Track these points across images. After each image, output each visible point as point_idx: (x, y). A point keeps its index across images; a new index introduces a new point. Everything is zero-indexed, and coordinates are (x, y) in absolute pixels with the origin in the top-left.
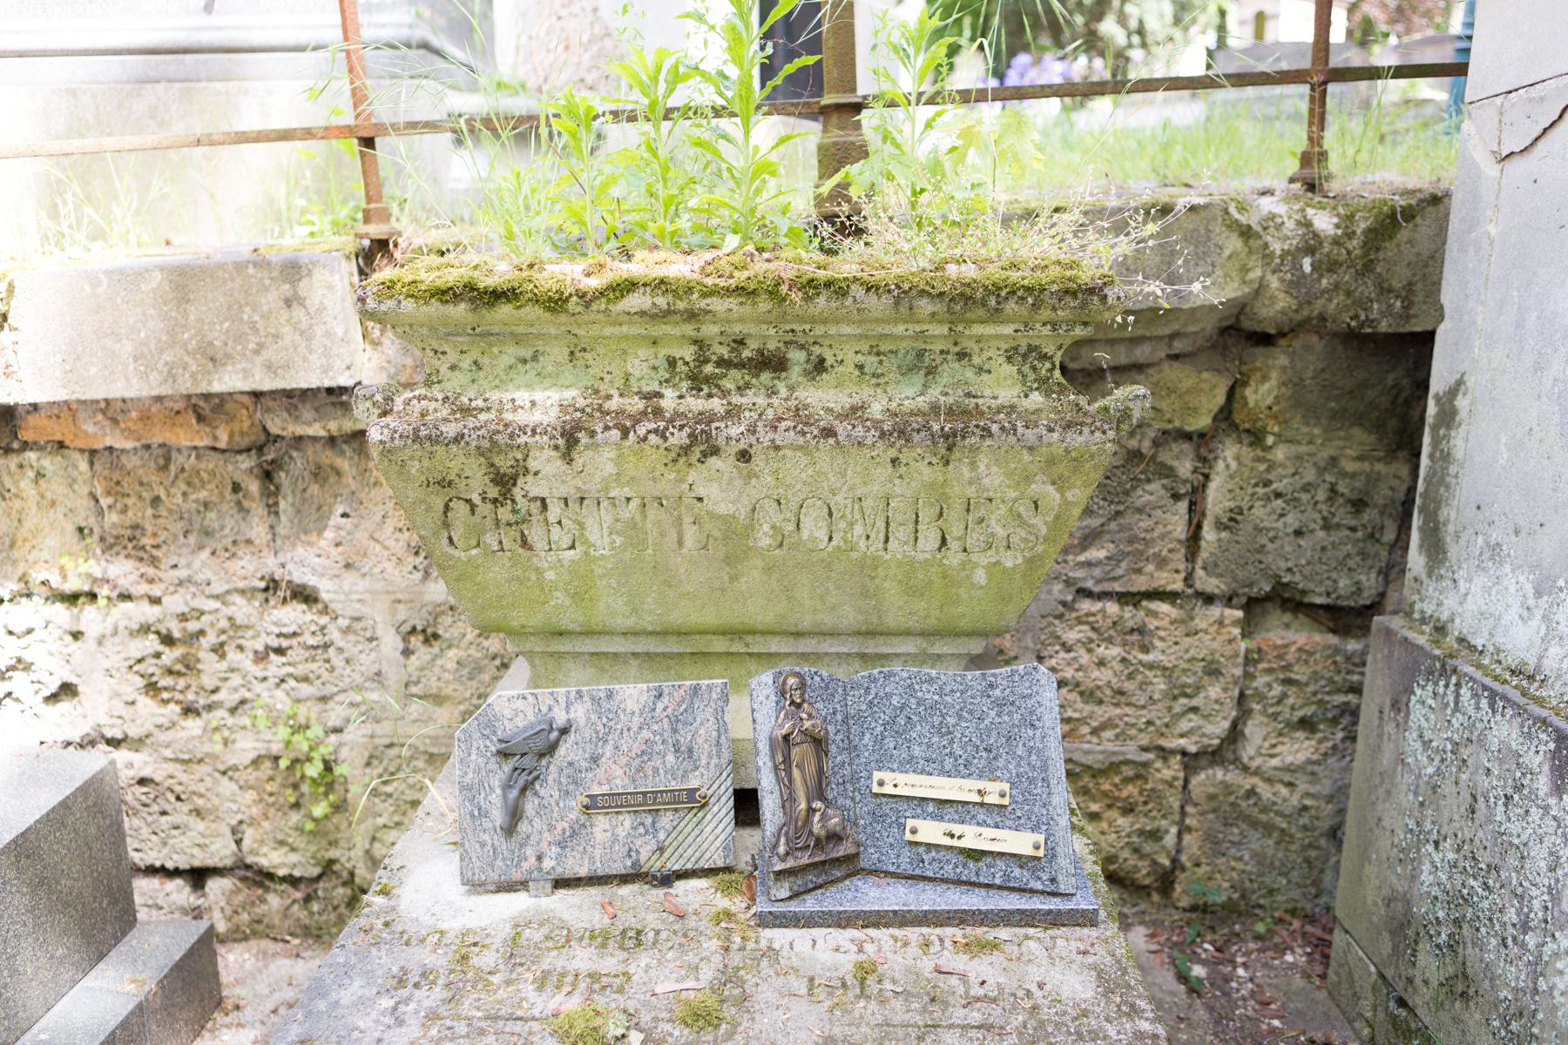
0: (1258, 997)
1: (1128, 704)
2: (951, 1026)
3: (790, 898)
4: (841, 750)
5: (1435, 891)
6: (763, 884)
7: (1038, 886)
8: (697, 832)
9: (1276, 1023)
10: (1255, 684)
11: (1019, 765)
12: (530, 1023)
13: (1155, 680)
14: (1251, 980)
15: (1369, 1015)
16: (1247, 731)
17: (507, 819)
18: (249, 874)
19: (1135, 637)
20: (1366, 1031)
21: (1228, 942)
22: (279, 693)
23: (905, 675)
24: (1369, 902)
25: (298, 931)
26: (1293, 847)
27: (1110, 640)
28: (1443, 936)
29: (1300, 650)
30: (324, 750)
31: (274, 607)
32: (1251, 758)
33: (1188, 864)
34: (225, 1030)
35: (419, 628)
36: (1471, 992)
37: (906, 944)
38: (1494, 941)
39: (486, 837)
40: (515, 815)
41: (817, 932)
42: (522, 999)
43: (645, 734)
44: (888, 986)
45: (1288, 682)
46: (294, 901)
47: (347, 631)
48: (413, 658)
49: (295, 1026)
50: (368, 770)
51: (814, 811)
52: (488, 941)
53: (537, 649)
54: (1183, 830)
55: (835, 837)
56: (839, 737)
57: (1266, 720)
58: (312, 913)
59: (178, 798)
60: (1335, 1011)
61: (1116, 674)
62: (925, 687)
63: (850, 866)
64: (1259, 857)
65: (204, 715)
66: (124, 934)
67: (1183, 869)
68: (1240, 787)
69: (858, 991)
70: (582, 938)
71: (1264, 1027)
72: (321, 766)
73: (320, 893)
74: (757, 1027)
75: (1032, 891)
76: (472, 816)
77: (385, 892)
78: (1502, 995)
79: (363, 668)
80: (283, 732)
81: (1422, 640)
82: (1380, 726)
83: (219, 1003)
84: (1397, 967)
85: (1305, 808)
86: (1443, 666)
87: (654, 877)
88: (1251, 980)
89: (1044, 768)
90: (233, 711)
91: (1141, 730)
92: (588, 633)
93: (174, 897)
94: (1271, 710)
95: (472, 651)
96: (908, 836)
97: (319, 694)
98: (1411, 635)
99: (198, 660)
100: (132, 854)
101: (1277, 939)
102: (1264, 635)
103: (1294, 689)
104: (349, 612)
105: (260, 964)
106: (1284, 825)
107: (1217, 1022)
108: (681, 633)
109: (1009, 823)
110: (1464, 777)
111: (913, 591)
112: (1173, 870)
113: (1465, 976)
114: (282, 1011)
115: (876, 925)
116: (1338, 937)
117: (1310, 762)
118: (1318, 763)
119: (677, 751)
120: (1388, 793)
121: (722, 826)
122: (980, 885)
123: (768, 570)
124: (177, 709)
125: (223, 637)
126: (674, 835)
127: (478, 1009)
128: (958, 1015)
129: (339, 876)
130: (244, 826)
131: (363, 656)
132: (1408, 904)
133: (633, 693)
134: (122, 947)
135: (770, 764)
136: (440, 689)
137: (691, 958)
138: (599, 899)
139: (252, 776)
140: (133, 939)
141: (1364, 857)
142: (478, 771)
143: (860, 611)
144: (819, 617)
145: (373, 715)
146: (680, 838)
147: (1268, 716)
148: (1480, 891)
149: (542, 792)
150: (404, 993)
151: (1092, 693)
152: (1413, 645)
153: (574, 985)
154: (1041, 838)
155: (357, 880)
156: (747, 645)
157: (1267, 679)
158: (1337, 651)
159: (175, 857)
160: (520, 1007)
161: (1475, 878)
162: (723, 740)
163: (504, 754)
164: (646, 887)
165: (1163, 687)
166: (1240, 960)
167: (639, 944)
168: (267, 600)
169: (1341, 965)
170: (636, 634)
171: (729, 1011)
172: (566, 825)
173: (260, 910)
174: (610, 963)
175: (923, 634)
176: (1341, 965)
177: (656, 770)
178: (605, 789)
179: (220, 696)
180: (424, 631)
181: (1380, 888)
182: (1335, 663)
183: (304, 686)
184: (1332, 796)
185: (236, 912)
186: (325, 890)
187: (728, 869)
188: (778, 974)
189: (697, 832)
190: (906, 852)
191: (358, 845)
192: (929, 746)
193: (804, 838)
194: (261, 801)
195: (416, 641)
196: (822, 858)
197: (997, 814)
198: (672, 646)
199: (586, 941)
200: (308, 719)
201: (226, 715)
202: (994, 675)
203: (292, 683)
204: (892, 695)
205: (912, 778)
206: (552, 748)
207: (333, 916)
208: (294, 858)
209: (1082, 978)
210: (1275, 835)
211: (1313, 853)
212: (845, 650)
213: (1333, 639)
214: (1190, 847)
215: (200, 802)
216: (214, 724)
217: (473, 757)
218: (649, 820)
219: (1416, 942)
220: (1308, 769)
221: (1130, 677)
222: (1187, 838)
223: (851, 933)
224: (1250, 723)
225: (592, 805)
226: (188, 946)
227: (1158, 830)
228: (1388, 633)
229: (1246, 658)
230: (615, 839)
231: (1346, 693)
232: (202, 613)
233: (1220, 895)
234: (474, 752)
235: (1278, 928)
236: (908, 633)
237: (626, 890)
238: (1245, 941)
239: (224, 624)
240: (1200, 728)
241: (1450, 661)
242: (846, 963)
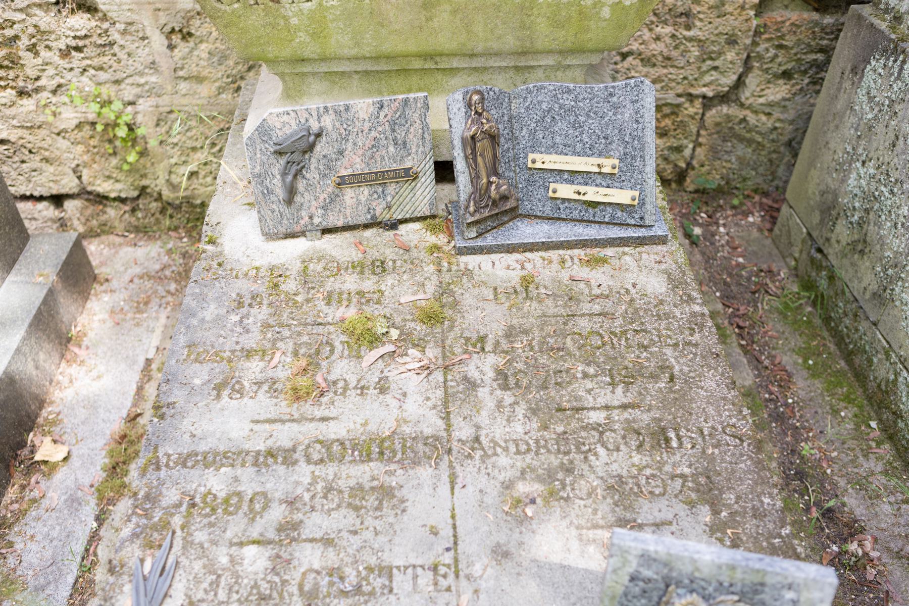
0: (731, 244)
1: (672, 66)
2: (583, 315)
3: (477, 237)
4: (507, 140)
5: (856, 191)
6: (457, 227)
7: (633, 222)
8: (411, 195)
9: (741, 260)
10: (758, 49)
11: (626, 147)
12: (328, 327)
13: (692, 49)
14: (727, 234)
15: (797, 255)
16: (747, 81)
17: (286, 195)
18: (91, 197)
19: (683, 19)
20: (793, 263)
21: (715, 212)
22: (84, 79)
23: (552, 88)
24: (810, 192)
25: (132, 229)
26: (763, 153)
27: (665, 22)
28: (856, 217)
29: (792, 24)
30: (126, 118)
31: (67, 17)
32: (747, 99)
33: (697, 166)
34: (104, 295)
35: (177, 29)
36: (867, 250)
37: (550, 262)
38: (889, 224)
39: (274, 206)
40: (291, 193)
41: (495, 257)
42: (319, 311)
43: (374, 134)
44: (543, 291)
45: (780, 47)
46: (125, 212)
47: (124, 33)
48: (176, 51)
49: (181, 336)
50: (158, 129)
51: (492, 183)
52: (288, 273)
53: (287, 71)
54: (697, 144)
55: (504, 198)
56: (505, 132)
57: (760, 73)
58: (138, 219)
59: (30, 152)
60: (775, 251)
61: (666, 46)
62: (565, 96)
63: (514, 214)
64: (740, 160)
65: (34, 95)
66: (24, 245)
67: (693, 168)
68: (737, 117)
69: (524, 295)
70: (347, 268)
71: (734, 263)
72: (126, 128)
73: (141, 206)
74: (467, 322)
75: (628, 225)
76: (263, 193)
77: (212, 242)
78: (886, 254)
79: (142, 59)
80: (95, 107)
81: (883, 26)
82: (840, 83)
83: (95, 278)
84: (821, 231)
85: (775, 128)
86: (896, 47)
87: (386, 225)
88: (727, 234)
89: (642, 149)
90: (54, 92)
91: (678, 83)
92: (324, 59)
93: (45, 213)
94: (765, 66)
95: (218, 45)
96: (551, 194)
97: (113, 79)
98: (876, 22)
99: (20, 57)
100: (10, 188)
101: (745, 208)
102: (770, 14)
103: (783, 52)
104: (123, 19)
105: (113, 251)
106: (760, 140)
107: (707, 262)
108: (389, 57)
109: (616, 184)
110: (893, 123)
111: (557, 23)
112: (686, 170)
113: (865, 241)
114: (136, 280)
115: (531, 250)
116: (785, 209)
117: (784, 99)
118: (789, 100)
119: (395, 144)
120: (837, 127)
121: (427, 190)
122: (595, 222)
123: (454, 12)
124: (14, 92)
125: (34, 40)
126: (396, 198)
127: (293, 319)
128: (586, 307)
129: (151, 196)
130: (80, 168)
131: (140, 50)
132: (836, 196)
133: (363, 106)
134: (26, 253)
135: (462, 154)
136: (199, 72)
137: (418, 278)
138: (352, 240)
139: (79, 135)
140: (31, 248)
141: (811, 164)
142: (263, 164)
143: (518, 39)
144: (489, 44)
145: (153, 92)
146: (401, 200)
147: (763, 71)
148: (887, 194)
149: (308, 176)
150: (244, 311)
151: (649, 60)
152: (876, 29)
153: (349, 300)
154: (637, 193)
155: (164, 198)
156: (436, 63)
157: (767, 45)
158: (817, 24)
159: (39, 189)
160: (319, 317)
161: (885, 186)
162: (426, 135)
163: (280, 153)
164: (381, 230)
165: (697, 53)
166: (721, 222)
167: (384, 270)
168: (59, 11)
169: (783, 226)
170: (357, 58)
171: (448, 313)
172: (326, 196)
173: (103, 218)
174: (368, 284)
175: (561, 52)
176: (783, 226)
177: (382, 157)
178: (349, 172)
179: (42, 82)
180: (180, 31)
181: (819, 184)
182: (814, 32)
183: (101, 73)
184: (794, 120)
185: (88, 220)
186: (144, 204)
187: (433, 217)
188: (474, 287)
189: (411, 195)
190: (549, 203)
191: (161, 177)
192: (566, 136)
193: (485, 200)
194: (88, 151)
195: (176, 38)
196: (497, 211)
197: (608, 179)
198: (384, 66)
199: (350, 271)
200: (109, 96)
201: (50, 95)
202: (613, 87)
203: (92, 72)
204: (542, 102)
205: (554, 157)
206: (311, 147)
207: (152, 219)
208: (119, 186)
209: (659, 279)
210: (754, 146)
211: (774, 156)
212: (505, 64)
213: (815, 16)
214: (700, 155)
215: (47, 154)
216: (43, 102)
217: (258, 156)
218: (380, 190)
219: (837, 219)
220: (781, 105)
221: (676, 47)
222: (698, 150)
223: (516, 256)
224: (750, 75)
225: (342, 182)
226: (68, 250)
227: (681, 146)
228: (860, 18)
229: (756, 31)
230: (359, 203)
231: (816, 53)
232: (14, 23)
233: (715, 180)
234: (258, 152)
235: (745, 201)
236: (550, 52)
237: (368, 233)
238: (726, 210)
239: (31, 30)
240: (717, 80)
241: (902, 45)
242: (515, 276)
